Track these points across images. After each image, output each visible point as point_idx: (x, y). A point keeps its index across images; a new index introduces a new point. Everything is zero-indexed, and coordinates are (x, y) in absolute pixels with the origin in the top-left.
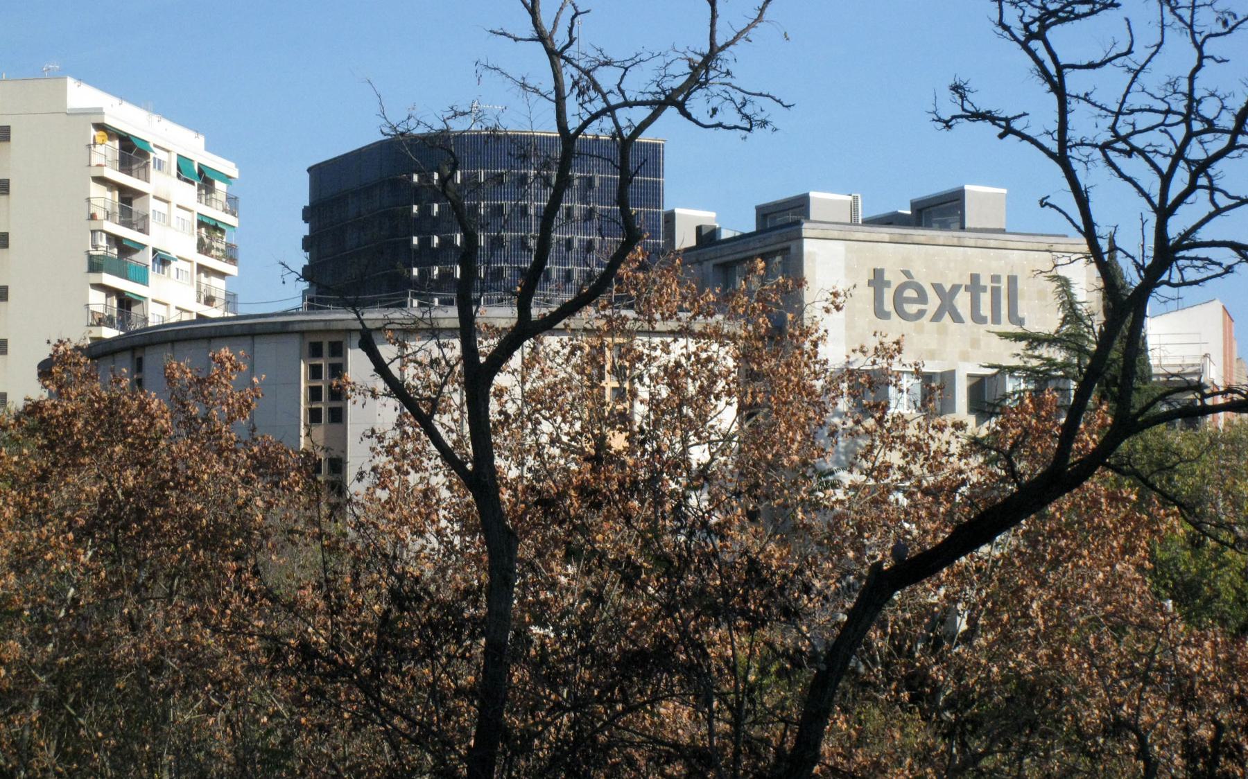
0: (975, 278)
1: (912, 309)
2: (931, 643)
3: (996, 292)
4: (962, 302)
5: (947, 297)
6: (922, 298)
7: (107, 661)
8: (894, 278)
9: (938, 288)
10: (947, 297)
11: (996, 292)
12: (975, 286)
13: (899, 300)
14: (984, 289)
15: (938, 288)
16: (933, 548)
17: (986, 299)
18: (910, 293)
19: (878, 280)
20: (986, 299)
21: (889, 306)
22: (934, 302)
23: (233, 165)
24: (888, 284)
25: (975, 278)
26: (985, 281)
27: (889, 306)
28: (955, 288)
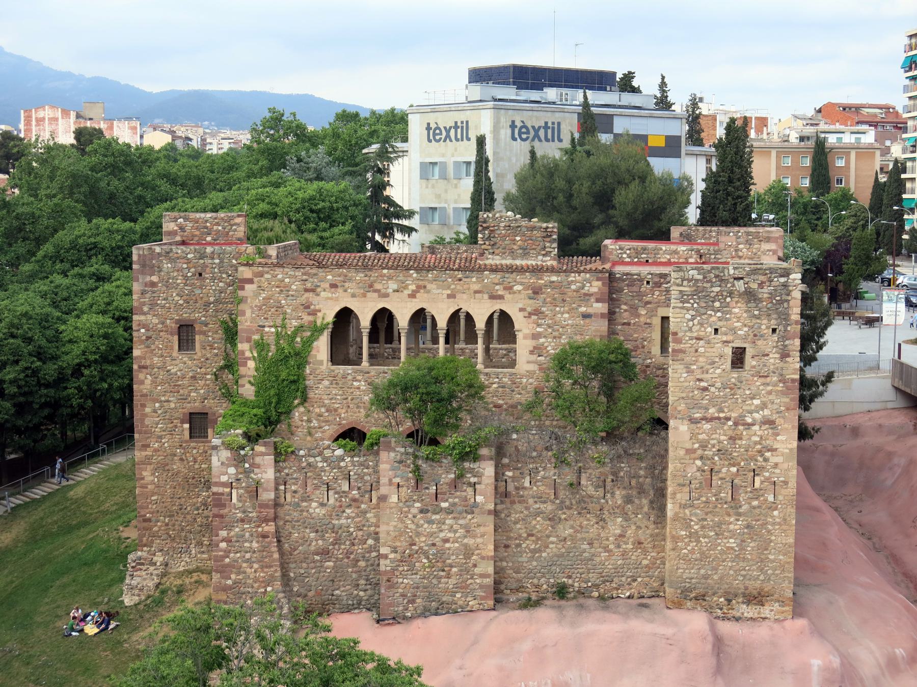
0: (546, 123)
1: (524, 136)
2: (464, 584)
3: (553, 129)
4: (542, 133)
5: (448, 131)
6: (528, 132)
7: (635, 220)
8: (433, 126)
9: (533, 127)
10: (537, 131)
11: (553, 129)
12: (546, 127)
13: (520, 133)
14: (549, 128)
15: (445, 128)
16: (812, 176)
17: (550, 131)
18: (524, 130)
19: (513, 126)
20: (550, 131)
21: (517, 136)
22: (532, 133)
23: (595, 112)
24: (516, 127)
25: (546, 123)
26: (550, 125)
27: (517, 136)
28: (539, 128)
